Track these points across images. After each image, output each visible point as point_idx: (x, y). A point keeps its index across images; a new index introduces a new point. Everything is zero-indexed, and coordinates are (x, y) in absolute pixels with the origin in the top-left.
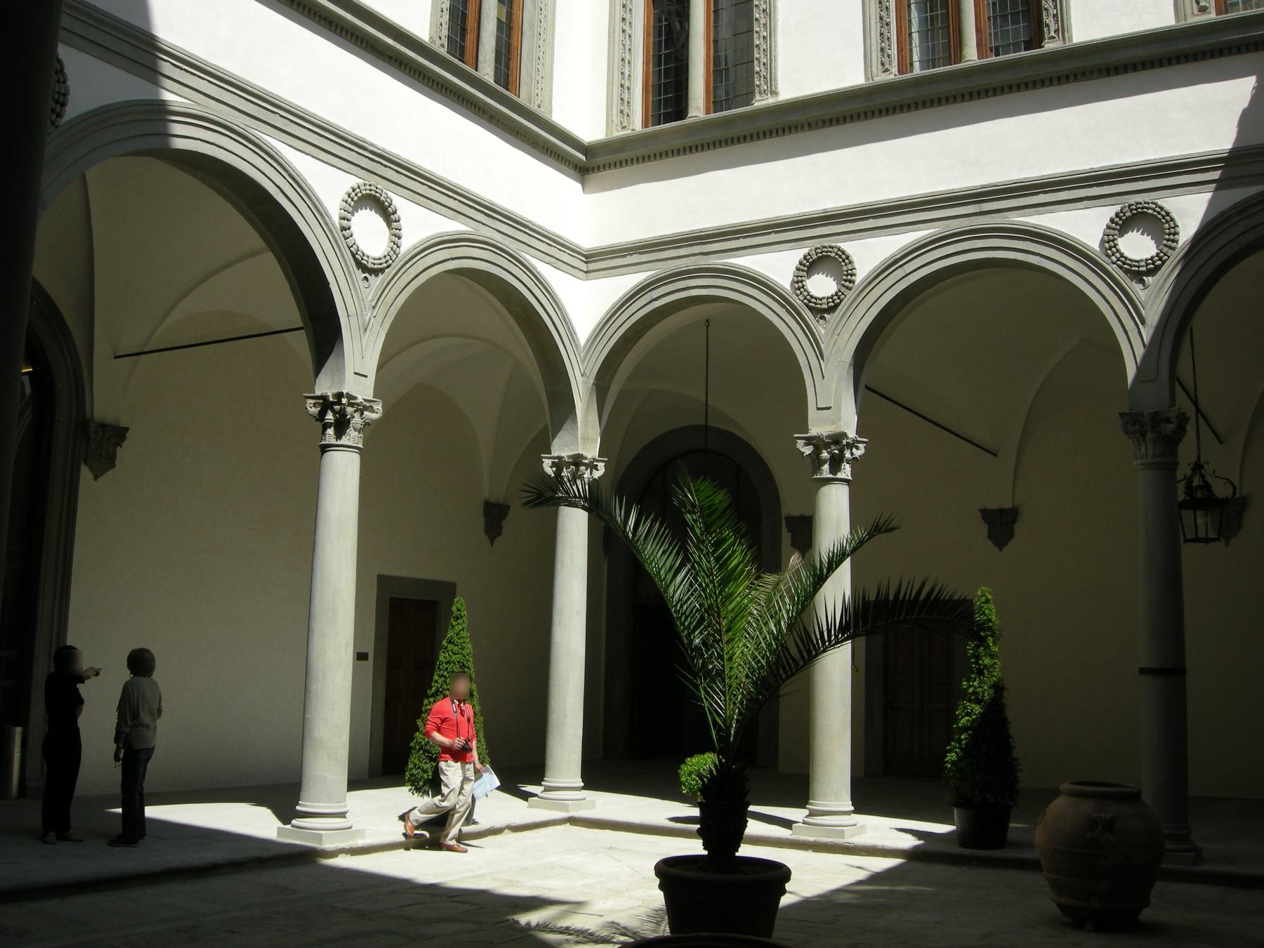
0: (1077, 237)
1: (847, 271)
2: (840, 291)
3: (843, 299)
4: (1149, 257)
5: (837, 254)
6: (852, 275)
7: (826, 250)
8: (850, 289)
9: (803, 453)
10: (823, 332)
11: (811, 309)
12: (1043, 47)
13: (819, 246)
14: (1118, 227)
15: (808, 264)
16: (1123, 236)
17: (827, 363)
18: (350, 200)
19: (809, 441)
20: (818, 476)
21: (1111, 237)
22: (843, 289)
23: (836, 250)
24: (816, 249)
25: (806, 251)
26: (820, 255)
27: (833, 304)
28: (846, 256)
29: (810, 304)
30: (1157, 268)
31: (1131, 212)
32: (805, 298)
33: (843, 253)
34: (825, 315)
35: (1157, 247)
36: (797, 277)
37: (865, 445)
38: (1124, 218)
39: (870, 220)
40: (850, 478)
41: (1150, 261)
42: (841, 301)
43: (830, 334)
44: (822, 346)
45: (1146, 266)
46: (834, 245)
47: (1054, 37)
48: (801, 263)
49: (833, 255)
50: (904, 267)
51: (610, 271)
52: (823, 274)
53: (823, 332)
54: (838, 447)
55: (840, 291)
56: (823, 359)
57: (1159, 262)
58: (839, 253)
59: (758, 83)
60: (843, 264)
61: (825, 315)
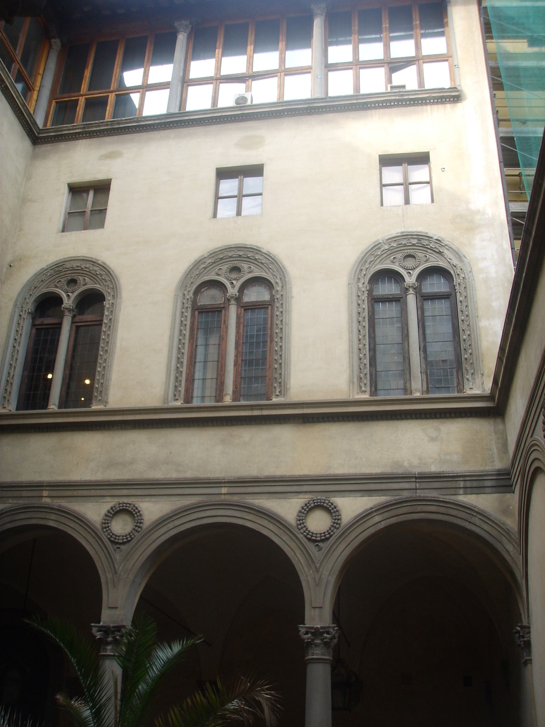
1: (137, 520)
4: (128, 533)
5: (132, 509)
6: (140, 523)
8: (139, 532)
10: (118, 558)
12: (272, 399)
15: (305, 512)
18: (303, 511)
19: (100, 629)
29: (313, 538)
30: (327, 539)
36: (105, 520)
41: (323, 535)
42: (132, 539)
47: (278, 395)
49: (130, 509)
55: (132, 533)
59: (96, 394)
60: (136, 515)
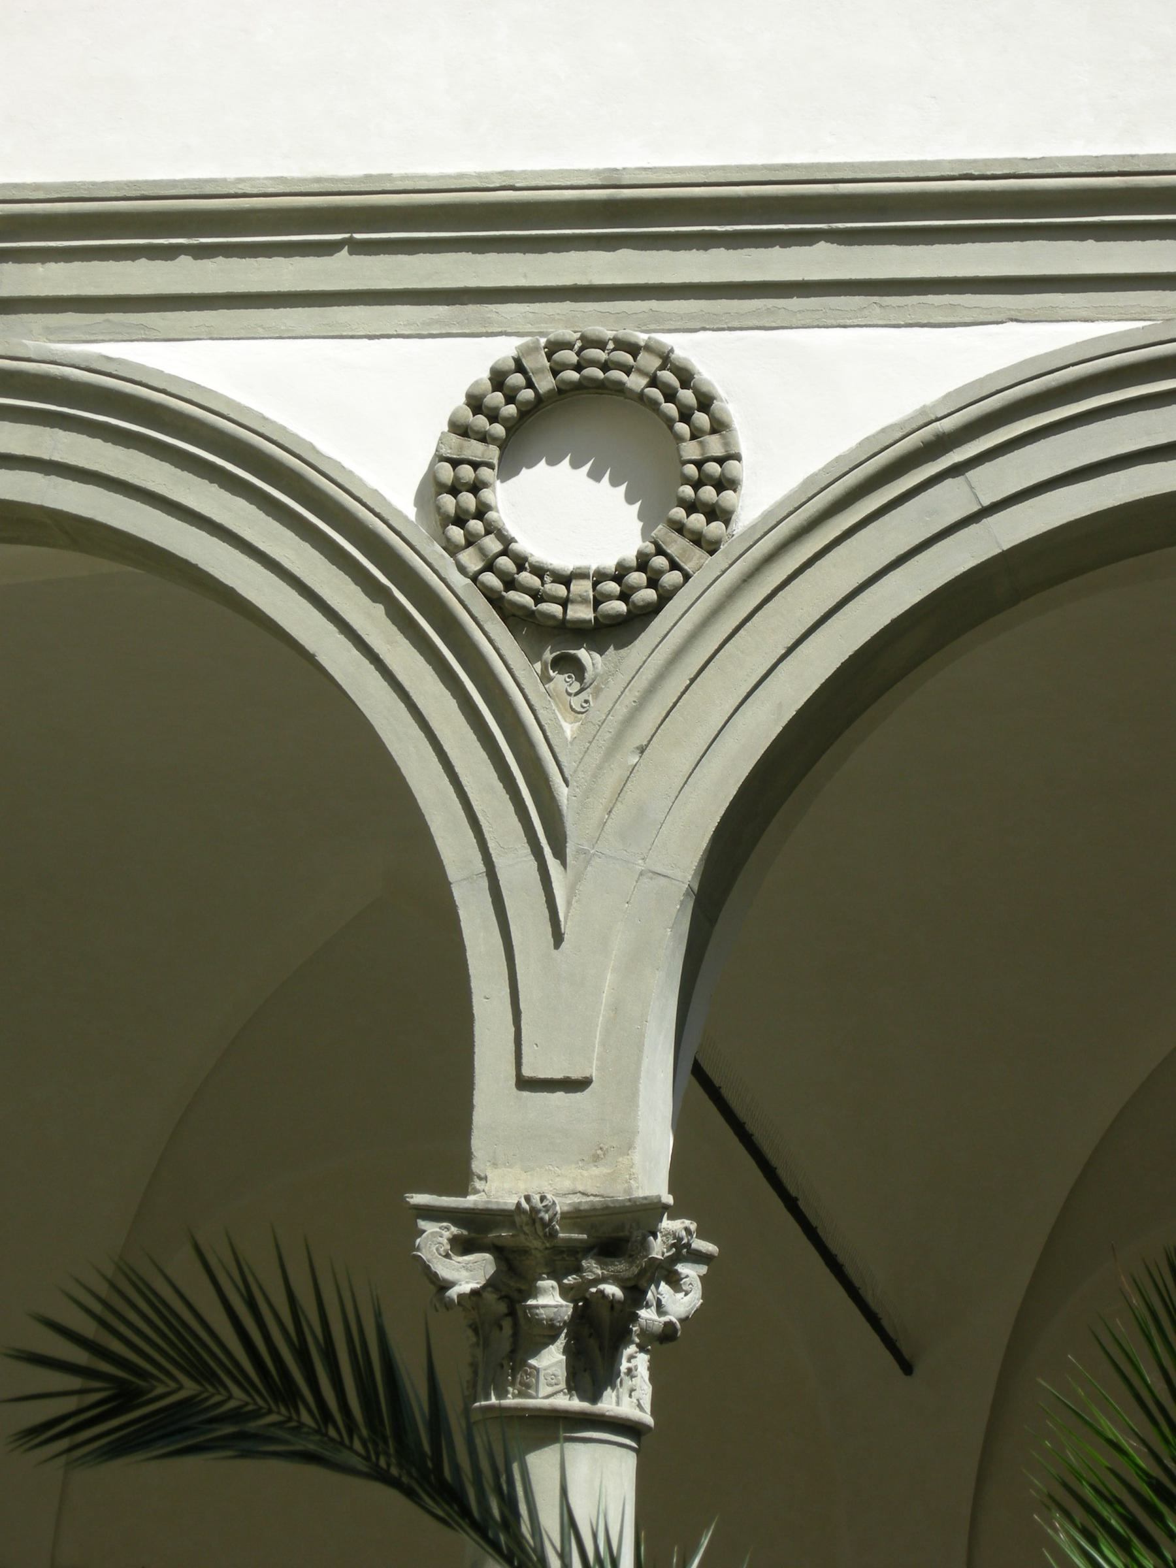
0: (348, 464)
1: (699, 464)
2: (660, 551)
3: (676, 589)
5: (654, 382)
7: (601, 355)
9: (445, 1285)
10: (569, 729)
11: (513, 617)
13: (571, 335)
14: (499, 430)
15: (511, 410)
16: (516, 472)
17: (578, 879)
20: (510, 1401)
21: (466, 472)
22: (677, 546)
23: (650, 362)
24: (553, 348)
25: (503, 349)
26: (573, 375)
27: (620, 607)
28: (699, 394)
29: (513, 595)
31: (555, 373)
32: (490, 567)
33: (686, 377)
34: (582, 654)
35: (645, 534)
37: (703, 1269)
38: (528, 394)
39: (822, 245)
40: (648, 1419)
42: (665, 598)
43: (606, 735)
44: (563, 793)
45: (597, 603)
46: (642, 338)
48: (475, 403)
49: (636, 382)
50: (973, 474)
51: (441, 311)
52: (575, 465)
53: (569, 729)
54: (621, 1267)
55: (660, 551)
56: (560, 854)
57: (650, 595)
58: (667, 376)
60: (682, 428)
61: (582, 654)
